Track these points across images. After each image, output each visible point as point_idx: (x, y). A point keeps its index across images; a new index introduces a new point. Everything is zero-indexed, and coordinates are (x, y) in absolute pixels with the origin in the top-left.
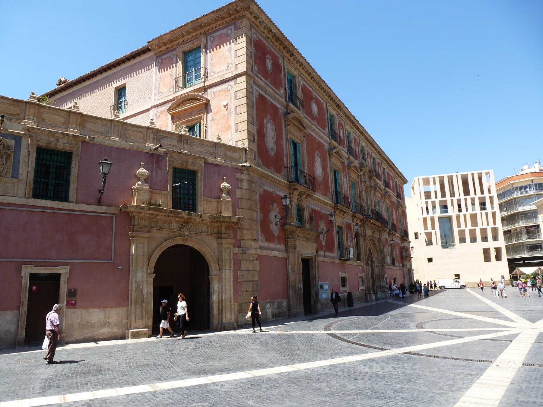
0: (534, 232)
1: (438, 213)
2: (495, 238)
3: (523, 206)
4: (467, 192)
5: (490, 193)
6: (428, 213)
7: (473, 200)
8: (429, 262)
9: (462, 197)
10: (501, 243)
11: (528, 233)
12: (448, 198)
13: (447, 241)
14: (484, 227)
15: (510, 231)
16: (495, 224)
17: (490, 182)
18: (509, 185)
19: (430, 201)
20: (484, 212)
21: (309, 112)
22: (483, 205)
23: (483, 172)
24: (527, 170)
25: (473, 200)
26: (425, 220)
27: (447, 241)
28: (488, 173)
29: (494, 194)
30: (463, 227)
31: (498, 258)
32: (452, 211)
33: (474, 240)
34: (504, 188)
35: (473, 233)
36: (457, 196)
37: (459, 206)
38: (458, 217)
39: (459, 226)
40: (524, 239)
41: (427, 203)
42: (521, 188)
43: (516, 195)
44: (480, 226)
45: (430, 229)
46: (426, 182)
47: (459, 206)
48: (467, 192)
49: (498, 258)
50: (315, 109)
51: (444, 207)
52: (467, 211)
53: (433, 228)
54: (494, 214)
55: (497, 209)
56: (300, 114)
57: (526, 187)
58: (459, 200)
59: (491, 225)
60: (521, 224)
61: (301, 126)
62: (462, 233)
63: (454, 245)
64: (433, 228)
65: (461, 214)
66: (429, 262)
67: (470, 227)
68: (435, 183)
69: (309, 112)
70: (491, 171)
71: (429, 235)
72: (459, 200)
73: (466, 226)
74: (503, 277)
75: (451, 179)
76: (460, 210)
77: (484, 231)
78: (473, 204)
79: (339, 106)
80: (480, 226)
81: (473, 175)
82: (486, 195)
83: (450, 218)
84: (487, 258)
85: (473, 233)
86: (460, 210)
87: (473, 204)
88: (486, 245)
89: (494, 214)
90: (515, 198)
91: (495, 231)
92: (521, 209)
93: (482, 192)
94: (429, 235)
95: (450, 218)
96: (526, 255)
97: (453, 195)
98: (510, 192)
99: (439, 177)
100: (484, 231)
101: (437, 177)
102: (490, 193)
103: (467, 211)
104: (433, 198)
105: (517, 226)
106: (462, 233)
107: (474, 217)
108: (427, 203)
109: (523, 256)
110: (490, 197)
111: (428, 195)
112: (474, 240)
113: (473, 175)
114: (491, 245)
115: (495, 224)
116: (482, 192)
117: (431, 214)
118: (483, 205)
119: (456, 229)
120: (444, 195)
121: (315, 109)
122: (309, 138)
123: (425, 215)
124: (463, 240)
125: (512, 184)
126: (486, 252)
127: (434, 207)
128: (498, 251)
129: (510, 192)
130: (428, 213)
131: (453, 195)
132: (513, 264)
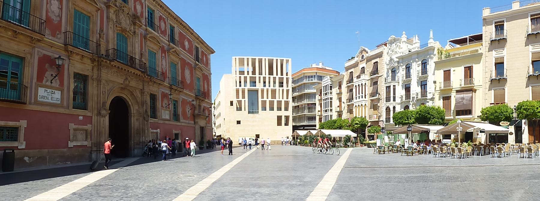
0: (312, 108)
1: (248, 86)
2: (286, 109)
3: (309, 89)
4: (271, 73)
5: (287, 75)
6: (240, 86)
7: (275, 78)
8: (240, 121)
9: (267, 76)
10: (290, 113)
11: (309, 108)
12: (257, 75)
13: (253, 110)
14: (280, 100)
15: (298, 106)
16: (287, 98)
17: (290, 70)
18: (301, 74)
19: (242, 76)
20: (281, 88)
21: (184, 48)
22: (281, 84)
23: (285, 59)
24: (314, 66)
25: (275, 78)
26: (237, 91)
27: (253, 110)
28: (287, 61)
29: (290, 76)
30: (265, 99)
31: (287, 124)
32: (259, 86)
33: (272, 109)
34: (298, 76)
35: (272, 103)
36: (264, 75)
37: (265, 82)
38: (263, 91)
39: (263, 97)
40: (306, 112)
41: (240, 77)
42: (309, 77)
43: (305, 81)
44: (277, 99)
45: (240, 99)
46: (242, 62)
47: (265, 82)
48: (271, 73)
49: (287, 124)
50: (186, 43)
51: (253, 83)
52: (269, 86)
53: (244, 97)
54: (288, 91)
55: (290, 99)
56: (179, 49)
57: (312, 77)
58: (264, 78)
59: (285, 99)
60: (306, 101)
61: (177, 53)
62: (264, 102)
63: (258, 112)
64: (244, 97)
65: (265, 88)
66: (240, 121)
67: (270, 99)
68: (248, 65)
69: (184, 48)
70: (290, 59)
71: (240, 102)
72: (264, 78)
73: (267, 98)
74: (288, 138)
75: (260, 61)
76: (265, 86)
77: (279, 103)
78: (274, 83)
79: (202, 42)
80: (277, 99)
81: (277, 60)
82: (285, 76)
83: (257, 91)
84: (279, 124)
85: (272, 103)
86: (265, 86)
87: (274, 83)
88: (279, 113)
89: (288, 91)
90: (304, 84)
91: (287, 103)
92: (306, 91)
93: (282, 74)
94: (240, 102)
95: (257, 91)
96: (305, 123)
97: (260, 73)
98: (301, 79)
99: (252, 59)
100: (279, 103)
101: (250, 58)
102: (287, 75)
103: (269, 86)
104: (246, 75)
105: (303, 102)
106: (264, 102)
107: (274, 92)
108: (240, 77)
109: (304, 124)
110: (287, 78)
111: (242, 73)
112: (272, 109)
113: (277, 60)
114: (283, 113)
115: (287, 98)
116: (282, 74)
117: (243, 87)
118: (281, 84)
119: (260, 99)
120: (254, 73)
121: (186, 43)
122: (182, 60)
123: (238, 87)
124: (264, 109)
125: (304, 73)
126: (279, 118)
127: (245, 82)
128: (287, 118)
129: (301, 79)
130: (240, 86)
131: (260, 73)
132: (295, 128)
